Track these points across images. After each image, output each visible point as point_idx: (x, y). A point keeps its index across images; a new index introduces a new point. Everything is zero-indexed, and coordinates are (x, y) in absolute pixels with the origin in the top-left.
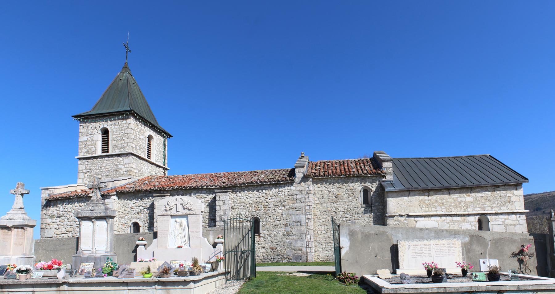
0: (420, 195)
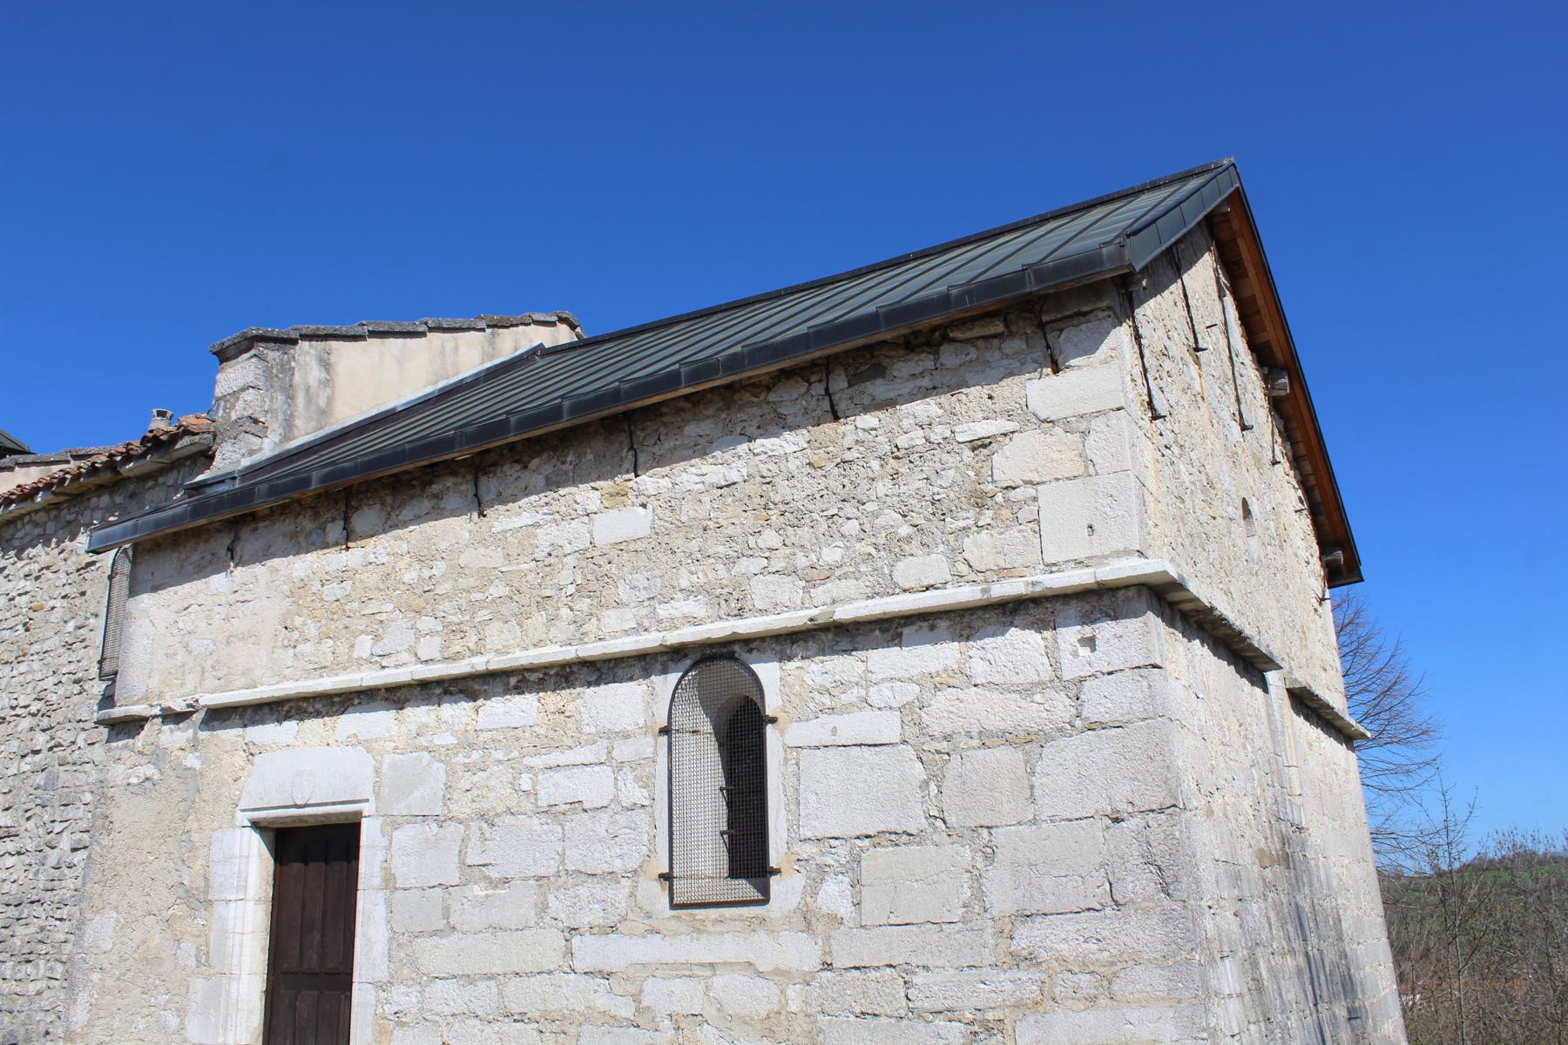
0: (299, 544)
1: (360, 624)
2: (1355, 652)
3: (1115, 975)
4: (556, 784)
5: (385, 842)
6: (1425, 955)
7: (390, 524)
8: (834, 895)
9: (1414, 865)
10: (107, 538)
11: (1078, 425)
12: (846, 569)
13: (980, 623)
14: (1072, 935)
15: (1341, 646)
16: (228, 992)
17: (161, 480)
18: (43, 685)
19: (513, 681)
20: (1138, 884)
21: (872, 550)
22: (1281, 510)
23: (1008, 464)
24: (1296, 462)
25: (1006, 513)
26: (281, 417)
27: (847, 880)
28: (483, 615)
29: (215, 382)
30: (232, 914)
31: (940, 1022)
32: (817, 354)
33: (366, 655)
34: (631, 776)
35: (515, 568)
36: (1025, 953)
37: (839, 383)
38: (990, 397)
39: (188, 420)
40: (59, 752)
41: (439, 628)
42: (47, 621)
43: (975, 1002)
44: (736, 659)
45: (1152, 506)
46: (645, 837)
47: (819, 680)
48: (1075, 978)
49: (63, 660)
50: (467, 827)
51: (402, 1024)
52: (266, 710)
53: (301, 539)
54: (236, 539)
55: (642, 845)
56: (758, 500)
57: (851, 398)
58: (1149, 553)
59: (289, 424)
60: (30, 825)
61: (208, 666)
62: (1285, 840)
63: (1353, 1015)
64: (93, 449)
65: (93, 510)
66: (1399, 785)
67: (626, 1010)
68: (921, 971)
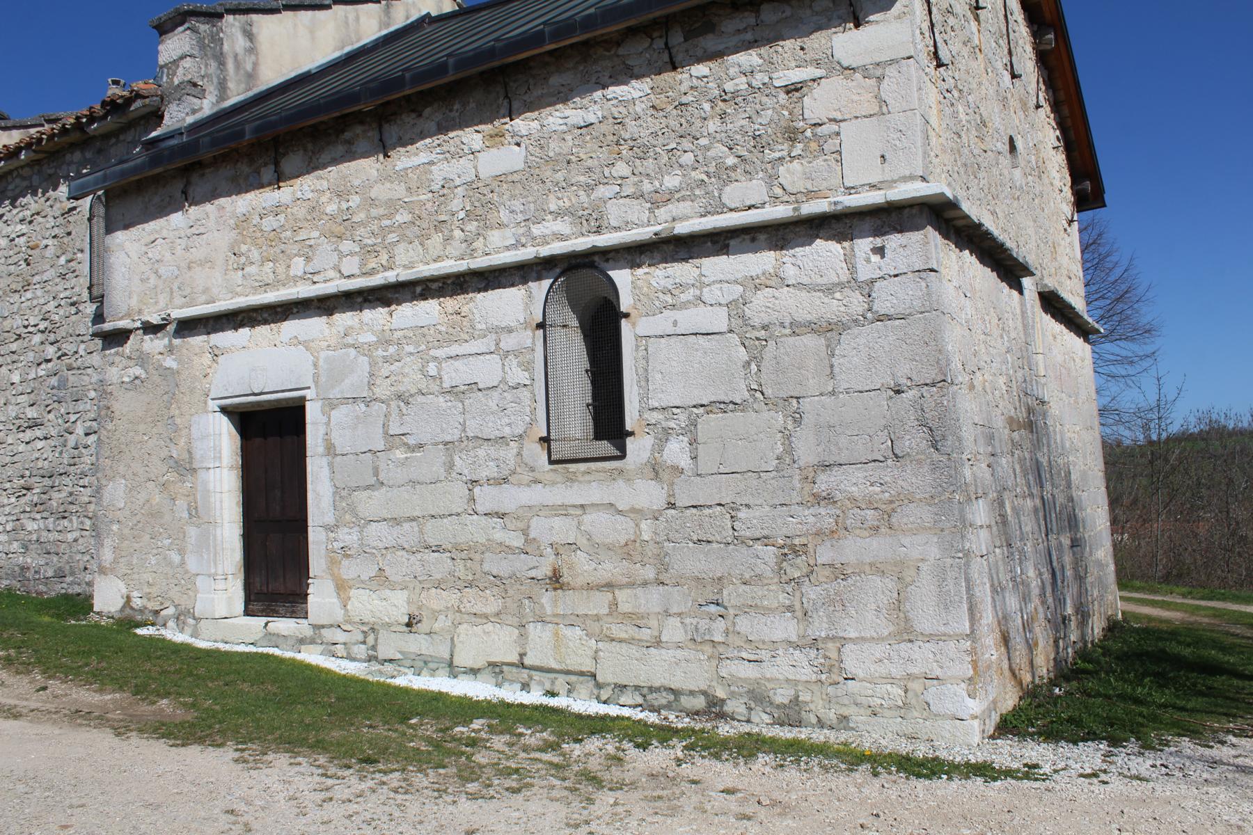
0: (240, 186)
1: (294, 249)
2: (1096, 267)
3: (894, 510)
4: (456, 370)
5: (325, 419)
6: (1135, 502)
7: (312, 166)
8: (676, 451)
9: (1130, 435)
10: (82, 187)
11: (874, 72)
12: (683, 193)
13: (791, 236)
14: (861, 480)
15: (1084, 261)
16: (215, 536)
17: (122, 137)
18: (46, 308)
19: (419, 289)
20: (913, 441)
21: (704, 177)
22: (1041, 147)
23: (816, 105)
24: (1056, 107)
25: (814, 145)
26: (215, 80)
27: (686, 439)
28: (392, 237)
29: (158, 52)
30: (212, 478)
31: (758, 547)
32: (658, 14)
33: (300, 274)
34: (515, 362)
35: (415, 198)
36: (824, 494)
37: (677, 38)
38: (802, 49)
39: (139, 85)
40: (66, 360)
41: (357, 250)
42: (43, 257)
43: (785, 531)
44: (596, 268)
45: (933, 140)
46: (528, 409)
47: (662, 282)
48: (862, 513)
49: (60, 288)
50: (389, 405)
51: (348, 556)
52: (224, 320)
53: (241, 181)
54: (188, 183)
55: (526, 414)
56: (611, 137)
57: (687, 51)
58: (930, 178)
59: (222, 87)
60: (51, 416)
61: (175, 288)
62: (1030, 410)
63: (1076, 544)
64: (62, 114)
65: (69, 164)
66: (1124, 373)
67: (517, 542)
68: (744, 509)
